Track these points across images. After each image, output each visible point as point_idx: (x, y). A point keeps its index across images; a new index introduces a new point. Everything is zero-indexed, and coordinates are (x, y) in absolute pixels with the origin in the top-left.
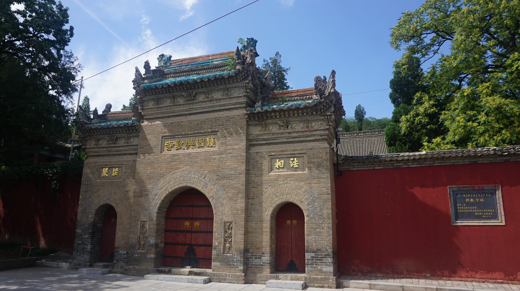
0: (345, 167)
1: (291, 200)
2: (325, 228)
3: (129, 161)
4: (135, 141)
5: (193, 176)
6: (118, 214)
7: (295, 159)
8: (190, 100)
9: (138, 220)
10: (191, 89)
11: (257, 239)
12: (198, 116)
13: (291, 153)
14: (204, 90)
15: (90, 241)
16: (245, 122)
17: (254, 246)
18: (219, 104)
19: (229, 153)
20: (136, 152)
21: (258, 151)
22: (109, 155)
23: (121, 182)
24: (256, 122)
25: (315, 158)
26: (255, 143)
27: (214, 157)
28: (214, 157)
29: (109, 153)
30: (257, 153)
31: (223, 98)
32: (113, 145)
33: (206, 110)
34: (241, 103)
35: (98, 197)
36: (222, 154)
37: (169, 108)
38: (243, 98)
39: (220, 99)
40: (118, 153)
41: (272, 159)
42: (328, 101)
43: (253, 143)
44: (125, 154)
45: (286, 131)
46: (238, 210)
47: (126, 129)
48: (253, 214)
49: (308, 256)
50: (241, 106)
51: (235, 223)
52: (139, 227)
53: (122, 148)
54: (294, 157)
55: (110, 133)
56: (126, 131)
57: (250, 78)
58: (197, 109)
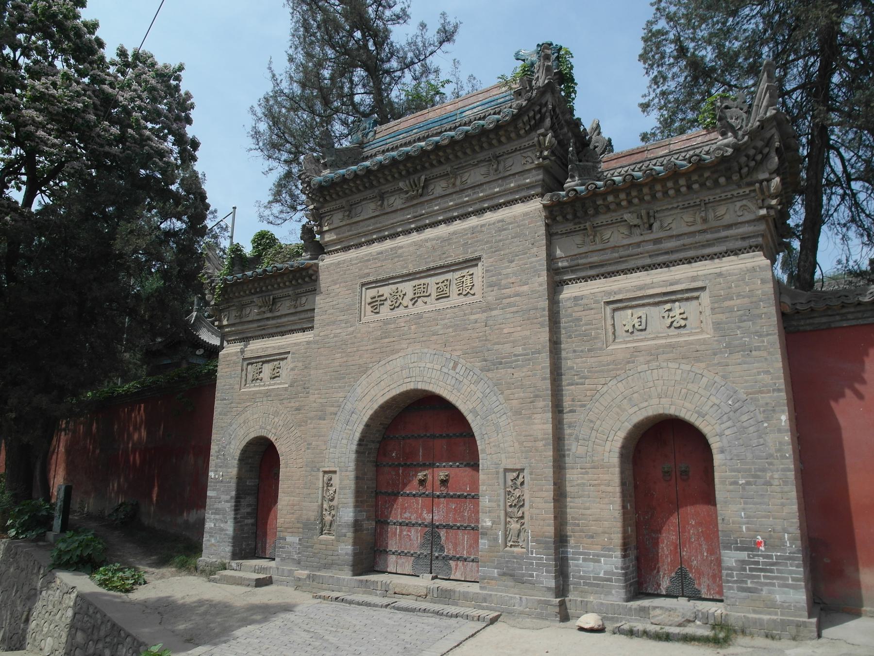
0: (816, 321)
1: (672, 411)
2: (776, 482)
9: (318, 470)
11: (588, 512)
13: (664, 290)
23: (286, 389)
24: (570, 226)
29: (263, 332)
31: (487, 180)
32: (269, 315)
36: (491, 310)
37: (373, 220)
39: (482, 184)
42: (760, 144)
45: (647, 238)
51: (531, 474)
54: (674, 301)
57: (548, 122)
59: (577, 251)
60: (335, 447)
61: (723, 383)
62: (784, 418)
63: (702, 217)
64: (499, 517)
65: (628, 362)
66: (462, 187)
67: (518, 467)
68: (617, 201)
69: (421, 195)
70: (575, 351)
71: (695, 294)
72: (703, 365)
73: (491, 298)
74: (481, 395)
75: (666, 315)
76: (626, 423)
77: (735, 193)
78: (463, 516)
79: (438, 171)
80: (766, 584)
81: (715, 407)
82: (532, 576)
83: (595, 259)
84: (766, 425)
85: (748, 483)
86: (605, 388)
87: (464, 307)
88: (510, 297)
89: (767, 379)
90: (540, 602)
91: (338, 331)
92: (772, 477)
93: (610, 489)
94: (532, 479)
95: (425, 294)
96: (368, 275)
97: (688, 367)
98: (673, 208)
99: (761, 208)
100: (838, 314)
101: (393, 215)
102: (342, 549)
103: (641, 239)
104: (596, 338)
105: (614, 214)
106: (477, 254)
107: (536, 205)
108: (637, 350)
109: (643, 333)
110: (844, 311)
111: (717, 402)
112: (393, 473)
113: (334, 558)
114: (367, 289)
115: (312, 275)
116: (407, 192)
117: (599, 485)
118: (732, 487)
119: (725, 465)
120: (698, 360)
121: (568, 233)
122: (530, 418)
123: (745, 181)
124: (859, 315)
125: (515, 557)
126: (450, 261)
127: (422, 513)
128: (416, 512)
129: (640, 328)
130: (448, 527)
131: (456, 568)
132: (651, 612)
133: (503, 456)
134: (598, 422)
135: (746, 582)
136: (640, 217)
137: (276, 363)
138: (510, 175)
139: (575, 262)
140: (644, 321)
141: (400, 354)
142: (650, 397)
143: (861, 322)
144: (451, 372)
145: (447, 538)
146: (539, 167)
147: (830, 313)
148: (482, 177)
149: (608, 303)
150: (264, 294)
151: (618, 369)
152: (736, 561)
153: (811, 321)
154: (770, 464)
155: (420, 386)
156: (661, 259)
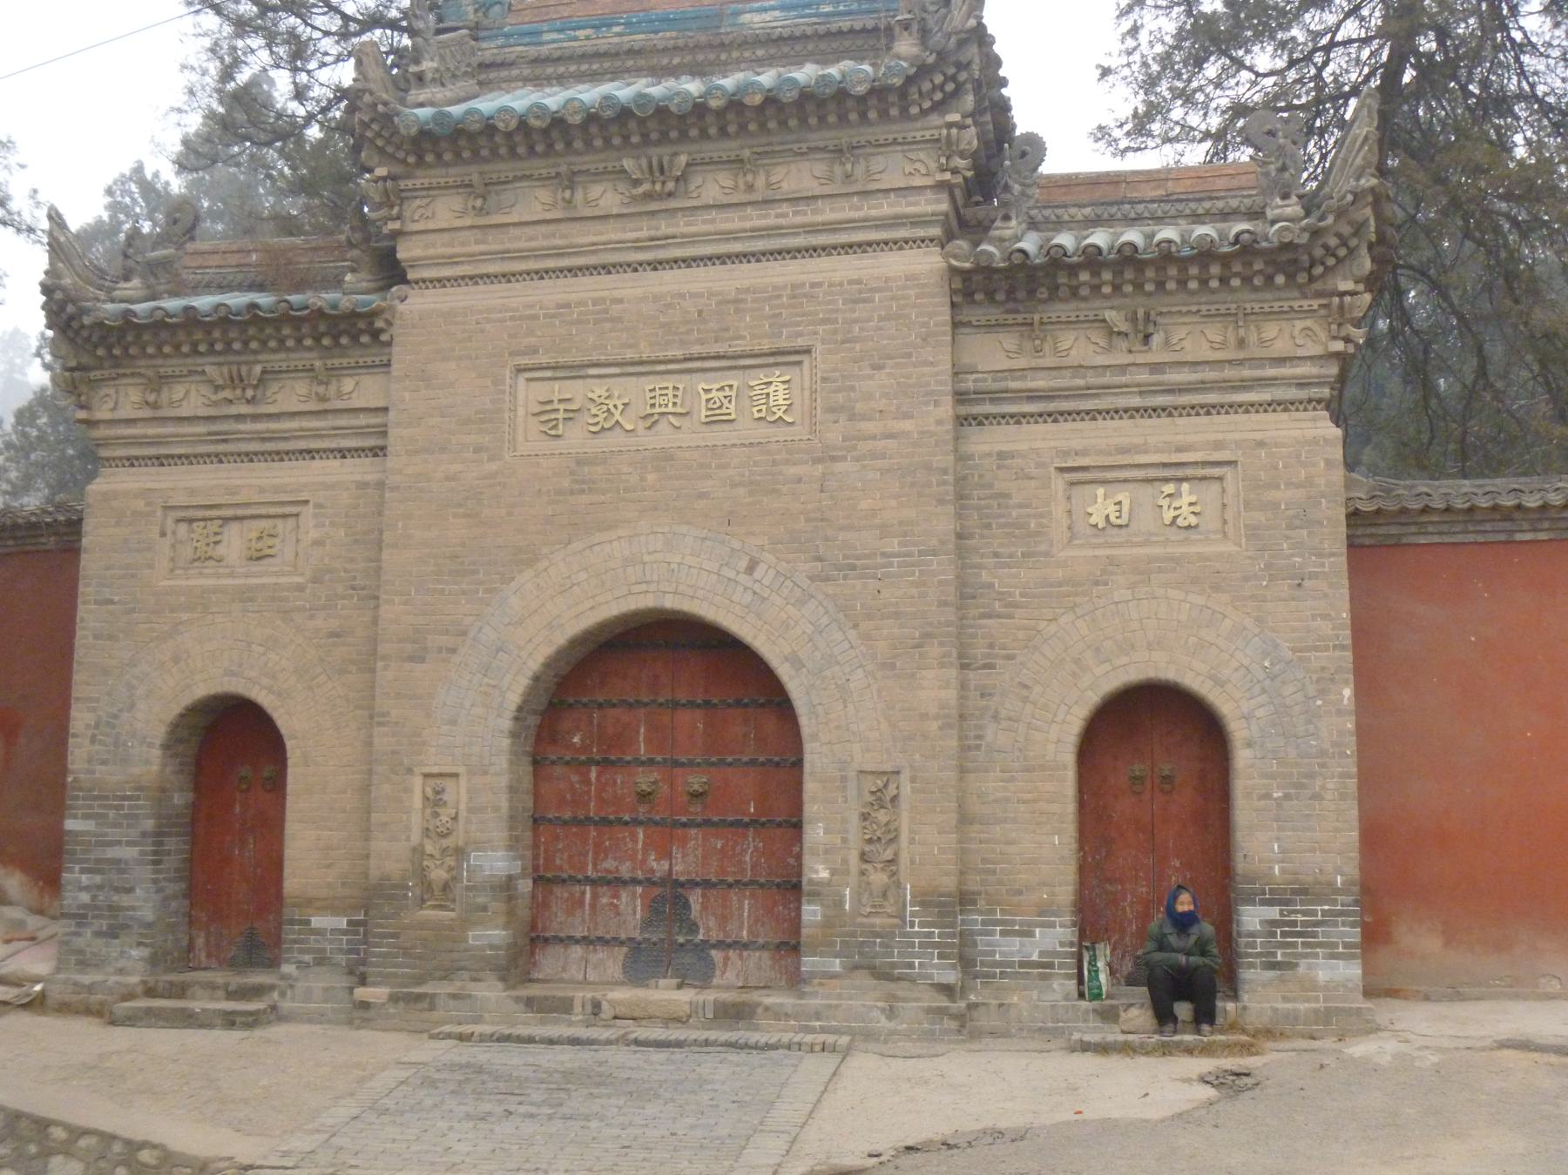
0: (1382, 530)
1: (1169, 674)
2: (1329, 796)
3: (332, 487)
4: (362, 390)
5: (690, 560)
6: (289, 744)
7: (1185, 486)
8: (660, 197)
9: (410, 771)
10: (664, 139)
11: (1012, 849)
12: (700, 272)
13: (1165, 458)
14: (729, 148)
15: (147, 872)
16: (947, 309)
17: (1000, 882)
18: (810, 218)
19: (874, 455)
20: (379, 442)
21: (1005, 448)
22: (219, 458)
23: (300, 588)
24: (995, 314)
25: (1277, 487)
26: (989, 408)
27: (793, 471)
28: (793, 471)
29: (221, 448)
30: (1001, 455)
31: (827, 190)
32: (244, 409)
33: (737, 247)
34: (917, 221)
35: (176, 660)
36: (834, 459)
37: (543, 229)
38: (929, 195)
39: (815, 198)
40: (269, 446)
41: (1072, 484)
42: (1346, 230)
43: (977, 409)
44: (310, 453)
45: (1140, 359)
46: (924, 717)
47: (322, 328)
48: (989, 736)
49: (1252, 917)
50: (921, 232)
51: (913, 780)
52: (417, 802)
53: (294, 424)
54: (1180, 480)
55: (228, 348)
56: (317, 339)
57: (969, 101)
58: (693, 239)
59: (1006, 364)
60: (453, 722)
61: (1257, 631)
62: (1347, 692)
63: (746, 183)
64: (845, 861)
65: (1097, 583)
66: (770, 194)
67: (888, 767)
68: (1096, 281)
69: (670, 195)
70: (996, 555)
71: (1216, 471)
72: (1225, 597)
73: (834, 435)
74: (809, 629)
75: (1165, 503)
76: (1090, 693)
77: (1296, 304)
78: (741, 862)
79: (712, 149)
80: (1306, 956)
81: (1243, 671)
82: (911, 966)
83: (1040, 383)
84: (1319, 702)
85: (1287, 797)
86: (1053, 628)
87: (774, 447)
88: (874, 438)
89: (1326, 628)
90: (929, 1011)
91: (459, 467)
92: (1323, 787)
93: (1055, 808)
94: (913, 790)
95: (679, 410)
96: (534, 351)
97: (1200, 600)
98: (1189, 312)
99: (1335, 338)
100: (1415, 523)
101: (598, 226)
102: (475, 938)
103: (1126, 359)
104: (1038, 533)
105: (1082, 305)
106: (800, 342)
107: (928, 263)
108: (1111, 560)
109: (1124, 531)
110: (1424, 519)
111: (1246, 662)
112: (575, 778)
113: (456, 955)
114: (529, 380)
115: (381, 331)
116: (636, 183)
117: (1034, 801)
118: (1262, 803)
119: (1252, 766)
120: (1216, 588)
121: (990, 327)
122: (913, 675)
123: (1318, 286)
124: (1445, 528)
125: (878, 935)
126: (739, 346)
127: (644, 861)
128: (633, 858)
129: (1119, 522)
130: (707, 884)
131: (725, 965)
132: (1123, 1014)
133: (857, 747)
134: (1037, 689)
135: (1274, 954)
136: (1133, 319)
137: (265, 524)
138: (879, 191)
139: (1003, 385)
140: (1126, 508)
141: (621, 533)
142: (1133, 647)
143: (1447, 539)
144: (742, 578)
145: (704, 908)
146: (941, 186)
147: (1403, 519)
148: (815, 183)
149: (1061, 470)
150: (231, 358)
151: (1076, 594)
152: (1261, 922)
153: (1373, 530)
154: (1322, 766)
155: (670, 603)
156: (1160, 400)
